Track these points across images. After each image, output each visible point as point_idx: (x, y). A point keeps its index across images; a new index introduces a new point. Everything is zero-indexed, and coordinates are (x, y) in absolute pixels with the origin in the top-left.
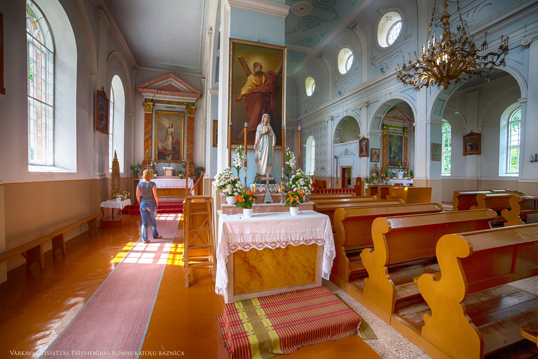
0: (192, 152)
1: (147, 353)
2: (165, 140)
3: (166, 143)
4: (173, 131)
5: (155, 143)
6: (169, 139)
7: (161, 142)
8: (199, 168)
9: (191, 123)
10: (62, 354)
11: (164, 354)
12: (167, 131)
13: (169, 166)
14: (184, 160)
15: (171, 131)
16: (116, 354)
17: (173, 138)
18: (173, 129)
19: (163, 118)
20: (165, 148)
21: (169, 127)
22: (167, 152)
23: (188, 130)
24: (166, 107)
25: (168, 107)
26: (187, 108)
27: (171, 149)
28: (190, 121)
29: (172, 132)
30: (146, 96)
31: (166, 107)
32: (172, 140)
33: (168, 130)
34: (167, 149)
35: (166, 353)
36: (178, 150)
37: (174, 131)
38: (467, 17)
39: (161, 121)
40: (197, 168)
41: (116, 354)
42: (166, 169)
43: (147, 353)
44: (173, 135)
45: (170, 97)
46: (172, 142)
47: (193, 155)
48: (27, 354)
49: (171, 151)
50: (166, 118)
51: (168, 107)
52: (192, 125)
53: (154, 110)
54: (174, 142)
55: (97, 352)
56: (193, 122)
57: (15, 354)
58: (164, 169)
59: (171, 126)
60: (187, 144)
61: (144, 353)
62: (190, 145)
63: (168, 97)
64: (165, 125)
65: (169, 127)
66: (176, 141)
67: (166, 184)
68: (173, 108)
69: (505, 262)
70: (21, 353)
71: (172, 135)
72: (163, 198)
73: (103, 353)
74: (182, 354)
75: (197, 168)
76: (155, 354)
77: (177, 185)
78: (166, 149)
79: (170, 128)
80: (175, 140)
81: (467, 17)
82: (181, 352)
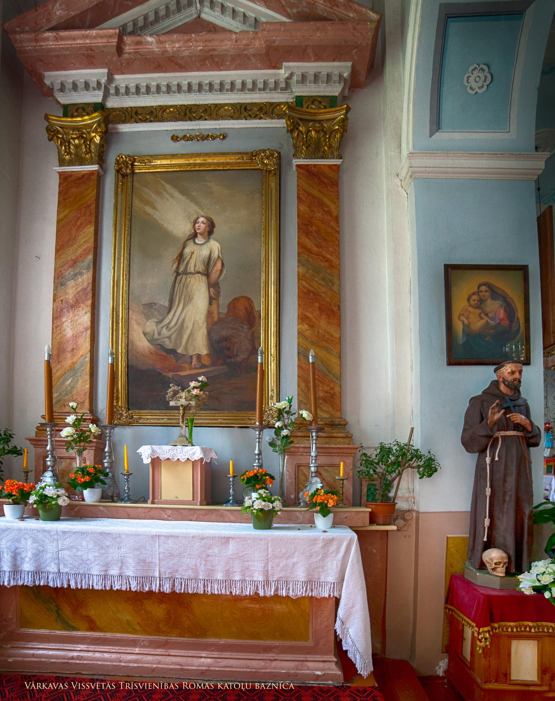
0: (334, 360)
2: (171, 302)
3: (173, 318)
4: (216, 254)
5: (115, 329)
6: (189, 299)
7: (148, 318)
8: (385, 451)
9: (322, 205)
12: (181, 257)
13: (189, 441)
14: (283, 404)
15: (205, 252)
17: (218, 293)
18: (214, 246)
19: (159, 193)
20: (169, 345)
21: (194, 236)
22: (180, 368)
23: (308, 242)
24: (175, 138)
25: (185, 138)
26: (293, 128)
27: (204, 351)
28: (315, 192)
29: (208, 262)
30: (62, 89)
31: (175, 138)
32: (211, 300)
33: (187, 251)
34: (180, 351)
36: (242, 357)
37: (222, 251)
39: (148, 209)
40: (373, 454)
42: (156, 462)
44: (214, 276)
45: (195, 82)
46: (209, 314)
47: (340, 378)
48: (50, 688)
49: (206, 361)
50: (176, 194)
51: (185, 138)
52: (329, 213)
53: (112, 158)
54: (225, 311)
56: (337, 198)
57: (33, 688)
58: (147, 461)
59: (202, 226)
60: (303, 318)
62: (323, 323)
63: (185, 83)
64: (170, 228)
65: (194, 236)
66: (233, 305)
67: (143, 562)
68: (214, 138)
69: (521, 429)
70: (42, 686)
71: (207, 274)
72: (133, 643)
75: (373, 454)
77: (228, 572)
78: (173, 352)
79: (200, 240)
80: (224, 301)
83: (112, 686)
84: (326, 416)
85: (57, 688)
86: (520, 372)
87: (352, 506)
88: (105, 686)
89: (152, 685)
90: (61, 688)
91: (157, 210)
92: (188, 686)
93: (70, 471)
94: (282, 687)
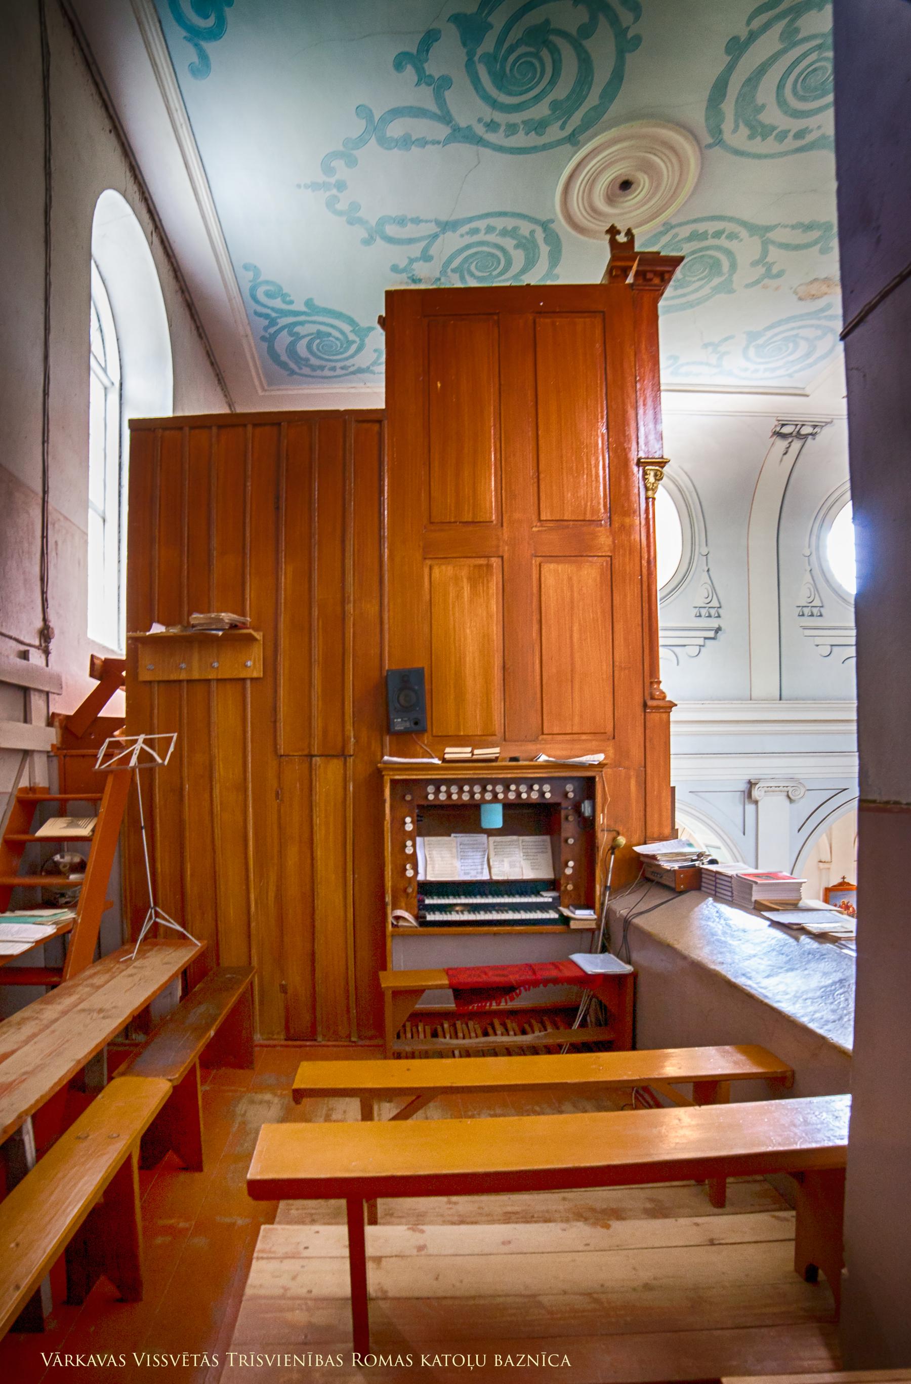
1: (459, 1360)
10: (199, 1363)
11: (509, 1364)
16: (363, 1362)
35: (515, 1360)
38: (744, 834)
41: (363, 1362)
43: (459, 1360)
48: (91, 1364)
55: (307, 1358)
57: (57, 1364)
61: (450, 1359)
70: (74, 1361)
73: (504, 1360)
74: (566, 1364)
76: (481, 1362)
81: (744, 834)
82: (562, 1358)
83: (118, 1361)
84: (846, 951)
85: (51, 1362)
86: (836, 285)
87: (203, 952)
88: (200, 1360)
89: (292, 1358)
90: (112, 1364)
91: (306, 187)
92: (362, 1360)
93: (656, 1127)
94: (68, 1363)
